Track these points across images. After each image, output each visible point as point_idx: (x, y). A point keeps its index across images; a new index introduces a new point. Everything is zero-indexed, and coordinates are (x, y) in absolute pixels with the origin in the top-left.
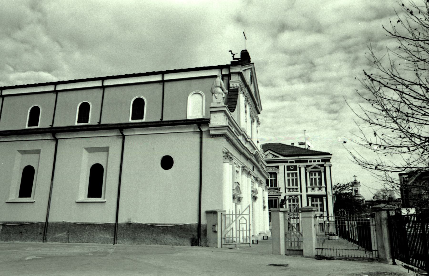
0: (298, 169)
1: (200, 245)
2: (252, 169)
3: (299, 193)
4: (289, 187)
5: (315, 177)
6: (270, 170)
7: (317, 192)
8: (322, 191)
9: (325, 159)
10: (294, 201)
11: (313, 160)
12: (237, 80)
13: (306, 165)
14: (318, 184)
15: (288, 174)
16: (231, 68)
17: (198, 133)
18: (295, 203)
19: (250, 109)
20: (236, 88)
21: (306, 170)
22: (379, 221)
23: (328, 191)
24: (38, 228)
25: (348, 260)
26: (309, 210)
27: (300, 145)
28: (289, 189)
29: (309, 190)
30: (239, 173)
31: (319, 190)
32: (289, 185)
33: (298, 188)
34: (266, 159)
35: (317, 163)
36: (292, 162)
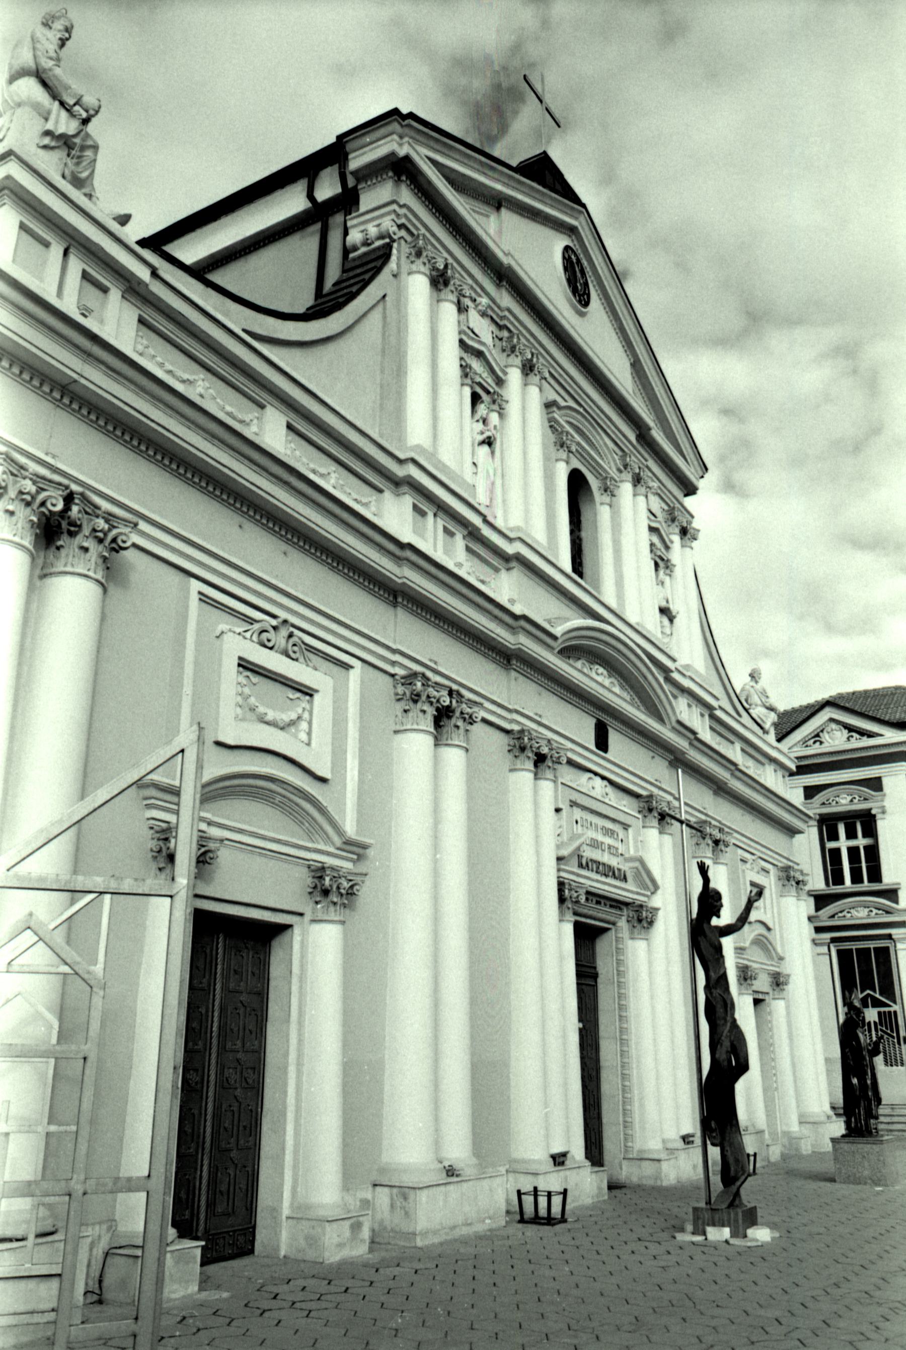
6: (843, 802)
19: (549, 405)
30: (317, 697)
34: (819, 751)
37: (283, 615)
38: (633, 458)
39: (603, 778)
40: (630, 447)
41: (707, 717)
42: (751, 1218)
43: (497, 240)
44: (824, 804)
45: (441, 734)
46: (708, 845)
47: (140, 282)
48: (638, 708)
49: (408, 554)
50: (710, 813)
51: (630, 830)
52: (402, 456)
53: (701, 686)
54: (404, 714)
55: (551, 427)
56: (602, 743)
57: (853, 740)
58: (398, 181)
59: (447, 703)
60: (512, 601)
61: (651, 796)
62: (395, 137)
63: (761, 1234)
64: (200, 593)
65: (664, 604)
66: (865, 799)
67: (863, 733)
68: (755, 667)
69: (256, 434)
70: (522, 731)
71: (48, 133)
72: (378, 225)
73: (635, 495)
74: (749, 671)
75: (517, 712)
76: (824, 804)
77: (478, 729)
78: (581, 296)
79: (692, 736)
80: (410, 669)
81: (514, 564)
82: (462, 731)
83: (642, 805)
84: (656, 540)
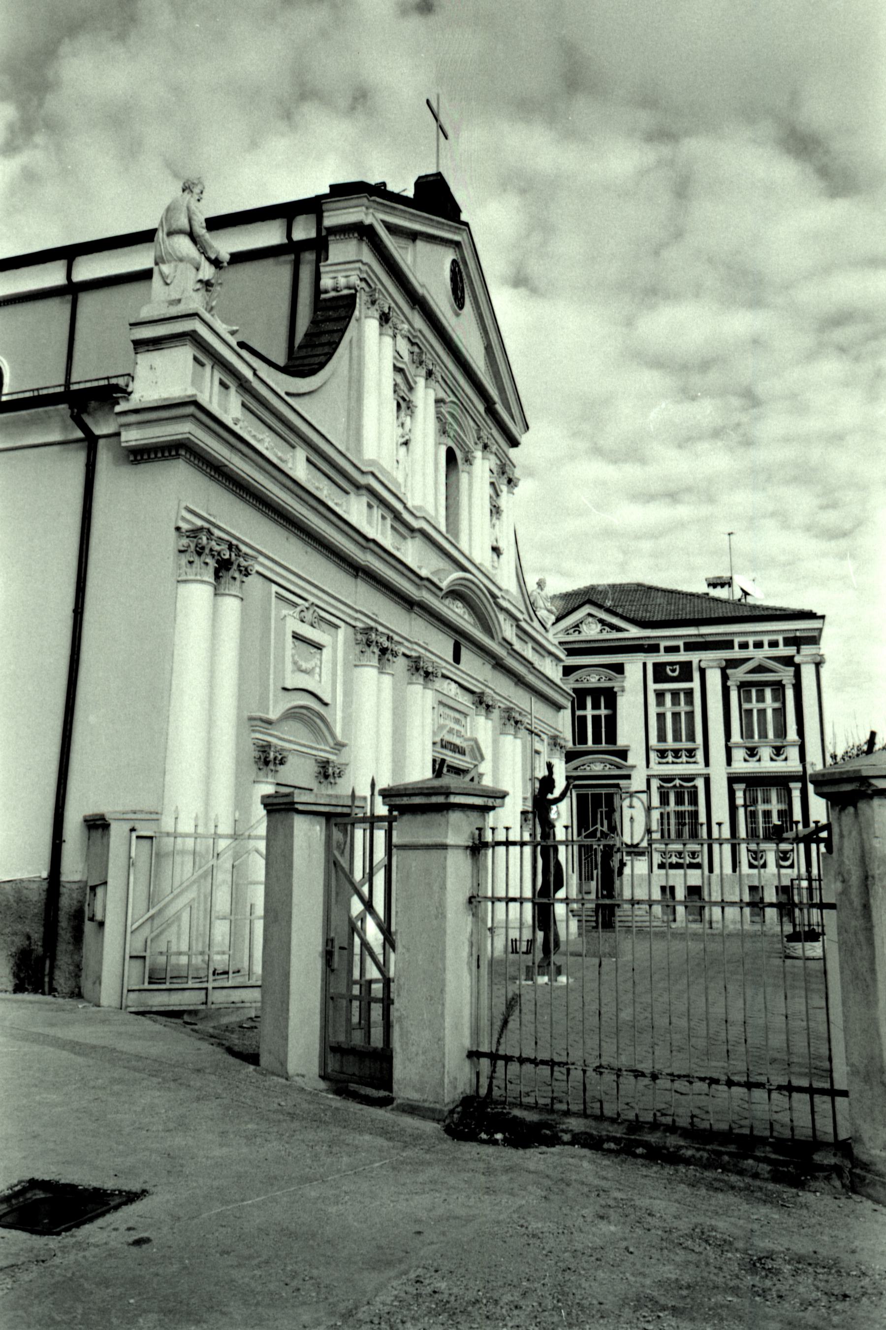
0: (696, 675)
1: (46, 989)
2: (449, 657)
3: (698, 768)
4: (662, 746)
5: (761, 706)
6: (593, 680)
7: (766, 765)
8: (786, 759)
9: (798, 634)
10: (679, 801)
11: (751, 640)
12: (354, 258)
13: (726, 660)
14: (771, 734)
15: (660, 695)
16: (328, 211)
17: (77, 450)
18: (687, 807)
19: (438, 401)
20: (345, 292)
21: (725, 678)
22: (855, 879)
23: (809, 759)
24: (785, 890)
25: (640, 1151)
26: (434, 800)
27: (711, 588)
28: (662, 753)
29: (739, 754)
30: (325, 650)
31: (774, 757)
32: (662, 738)
33: (694, 750)
34: (577, 639)
35: (767, 651)
36: (675, 649)
37: (312, 599)
38: (428, 355)
39: (456, 682)
40: (428, 346)
41: (514, 627)
42: (559, 972)
43: (412, 269)
44: (577, 680)
45: (219, 583)
46: (374, 653)
47: (247, 381)
48: (474, 626)
49: (371, 545)
50: (514, 701)
51: (468, 719)
52: (364, 469)
53: (514, 606)
54: (188, 565)
55: (438, 418)
56: (457, 659)
57: (605, 632)
58: (361, 239)
59: (227, 556)
60: (420, 567)
61: (483, 693)
62: (364, 209)
63: (563, 979)
64: (276, 593)
65: (495, 544)
66: (610, 679)
67: (613, 627)
68: (542, 577)
69: (291, 468)
70: (419, 657)
71: (200, 281)
72: (347, 277)
73: (381, 334)
74: (537, 580)
75: (416, 643)
76: (577, 680)
77: (253, 579)
78: (459, 302)
79: (509, 647)
80: (193, 523)
81: (418, 534)
82: (238, 583)
83: (411, 664)
84: (400, 380)
